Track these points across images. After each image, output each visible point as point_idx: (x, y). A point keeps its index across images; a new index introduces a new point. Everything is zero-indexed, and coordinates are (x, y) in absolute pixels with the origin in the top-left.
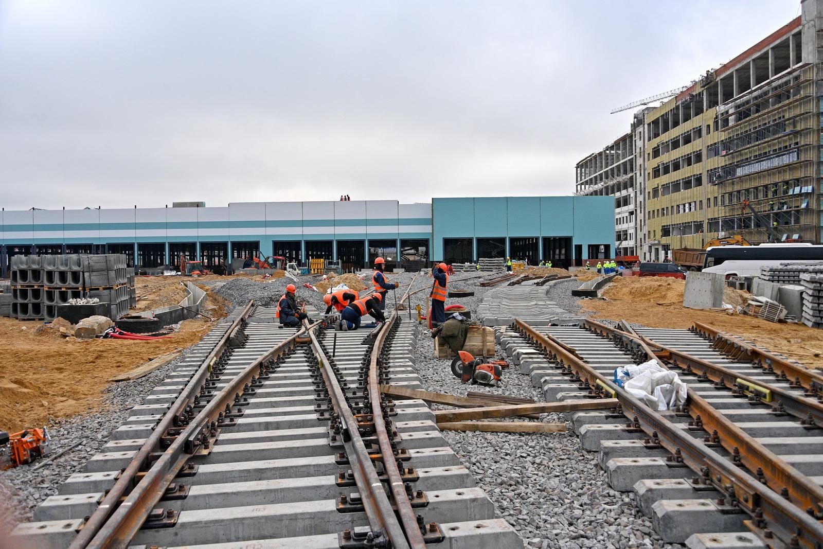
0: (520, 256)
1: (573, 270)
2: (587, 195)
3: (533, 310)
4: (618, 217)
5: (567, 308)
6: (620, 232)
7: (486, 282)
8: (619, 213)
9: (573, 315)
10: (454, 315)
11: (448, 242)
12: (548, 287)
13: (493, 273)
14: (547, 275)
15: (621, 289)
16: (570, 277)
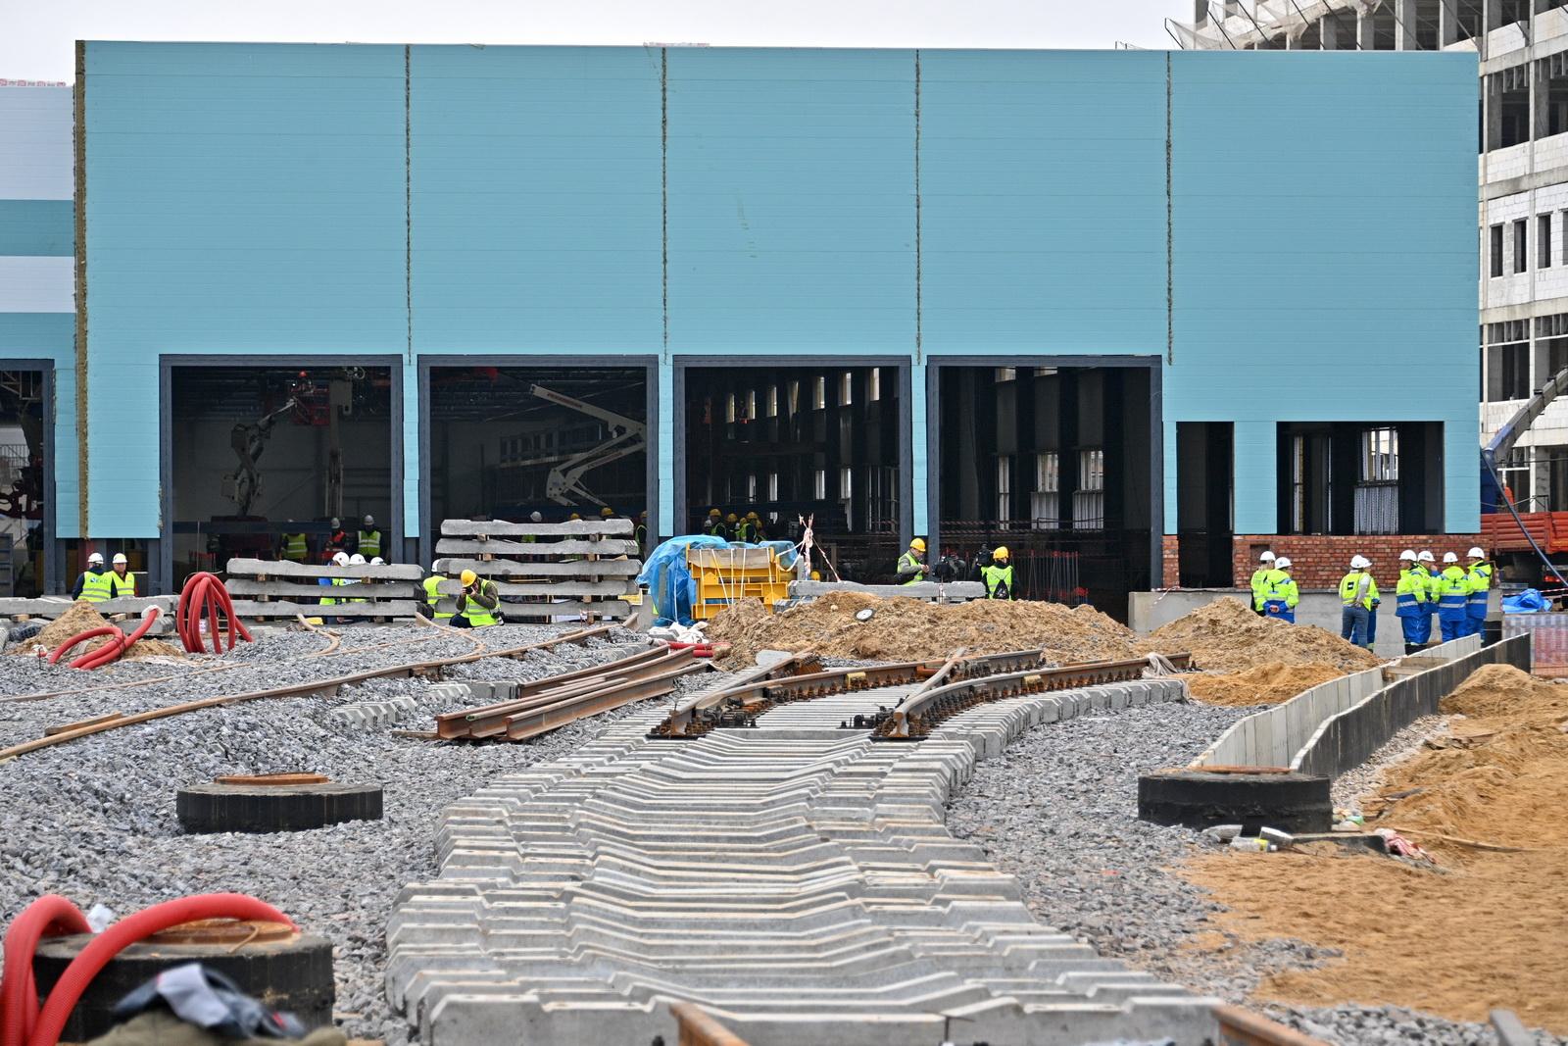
0: (763, 506)
1: (1162, 612)
2: (1278, 42)
3: (826, 933)
4: (1504, 212)
5: (1093, 919)
6: (1520, 326)
7: (486, 707)
8: (1515, 187)
9: (1133, 974)
10: (167, 983)
11: (198, 392)
12: (965, 750)
13: (548, 635)
14: (958, 655)
15: (1515, 764)
16: (1132, 670)
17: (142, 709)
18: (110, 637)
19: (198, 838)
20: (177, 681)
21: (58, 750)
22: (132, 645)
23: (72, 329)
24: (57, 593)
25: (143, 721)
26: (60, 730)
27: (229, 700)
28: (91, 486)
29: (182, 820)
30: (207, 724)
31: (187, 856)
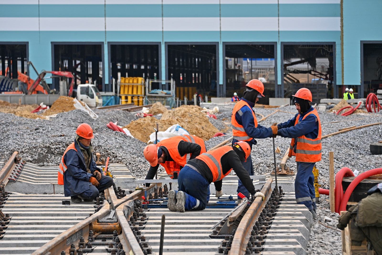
17: (360, 125)
18: (350, 108)
19: (375, 156)
20: (367, 119)
21: (342, 134)
22: (355, 110)
23: (340, 35)
24: (337, 98)
25: (361, 128)
26: (342, 130)
27: (380, 123)
28: (344, 73)
29: (371, 151)
30: (376, 129)
31: (373, 160)
